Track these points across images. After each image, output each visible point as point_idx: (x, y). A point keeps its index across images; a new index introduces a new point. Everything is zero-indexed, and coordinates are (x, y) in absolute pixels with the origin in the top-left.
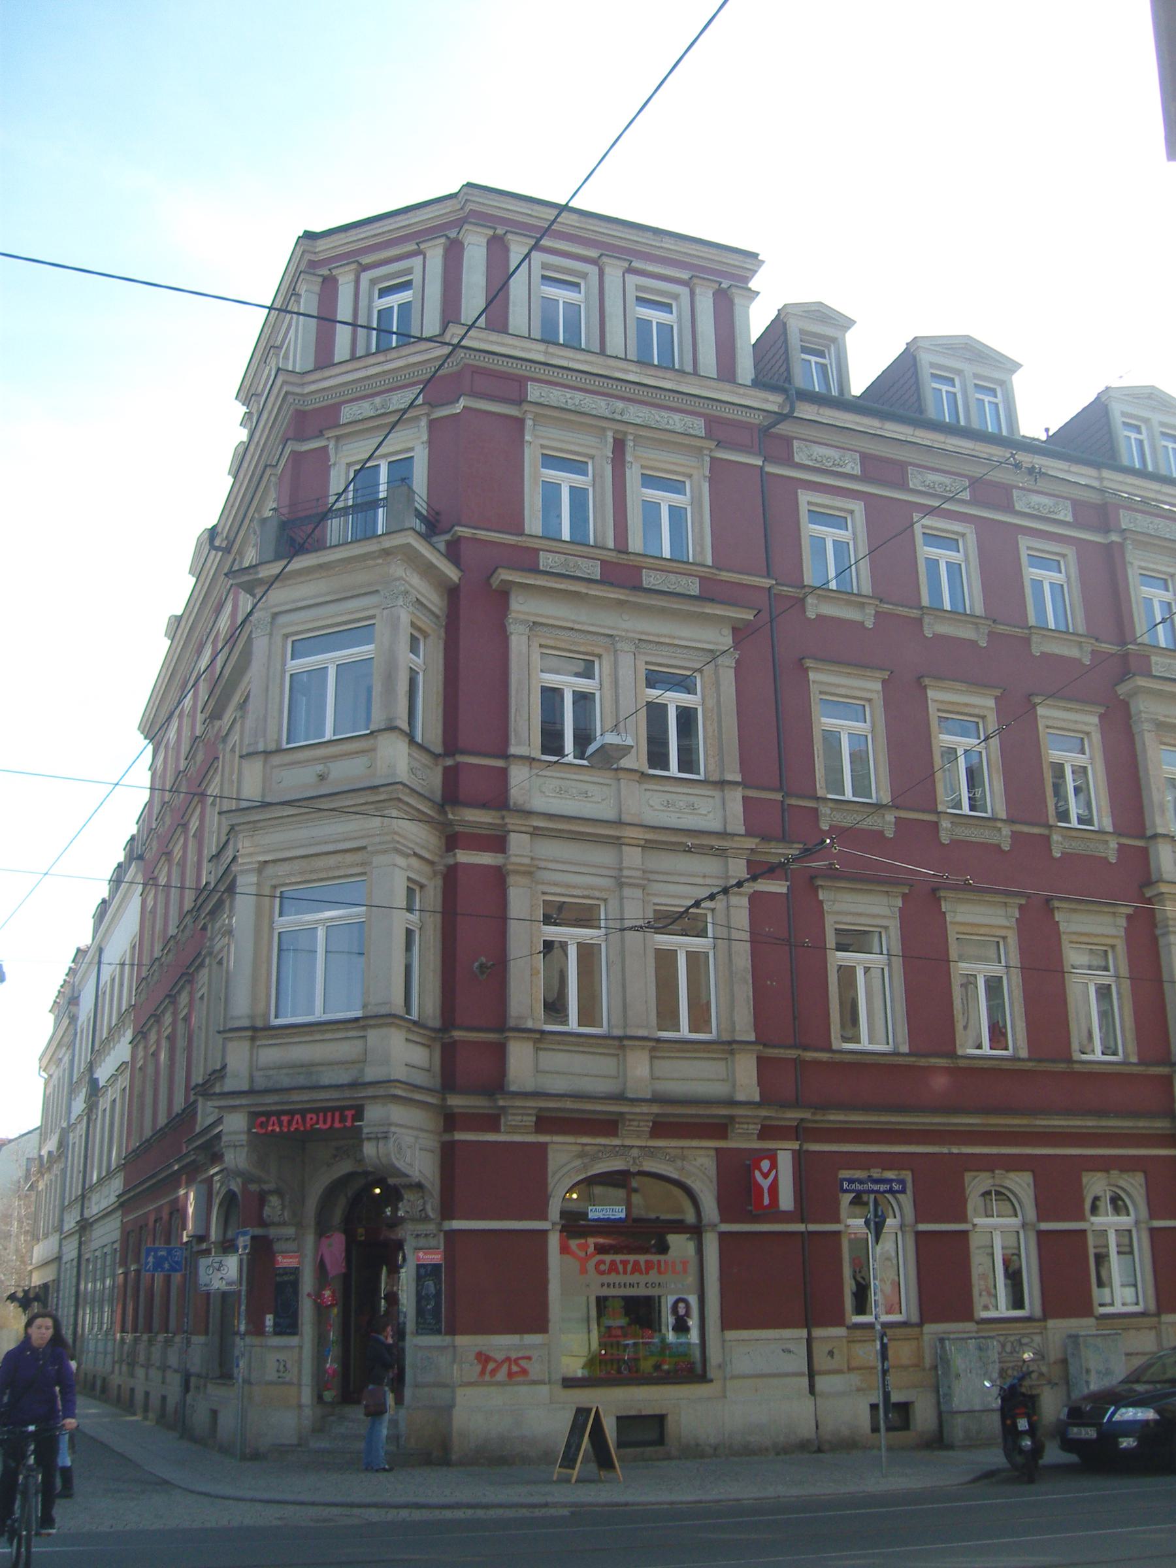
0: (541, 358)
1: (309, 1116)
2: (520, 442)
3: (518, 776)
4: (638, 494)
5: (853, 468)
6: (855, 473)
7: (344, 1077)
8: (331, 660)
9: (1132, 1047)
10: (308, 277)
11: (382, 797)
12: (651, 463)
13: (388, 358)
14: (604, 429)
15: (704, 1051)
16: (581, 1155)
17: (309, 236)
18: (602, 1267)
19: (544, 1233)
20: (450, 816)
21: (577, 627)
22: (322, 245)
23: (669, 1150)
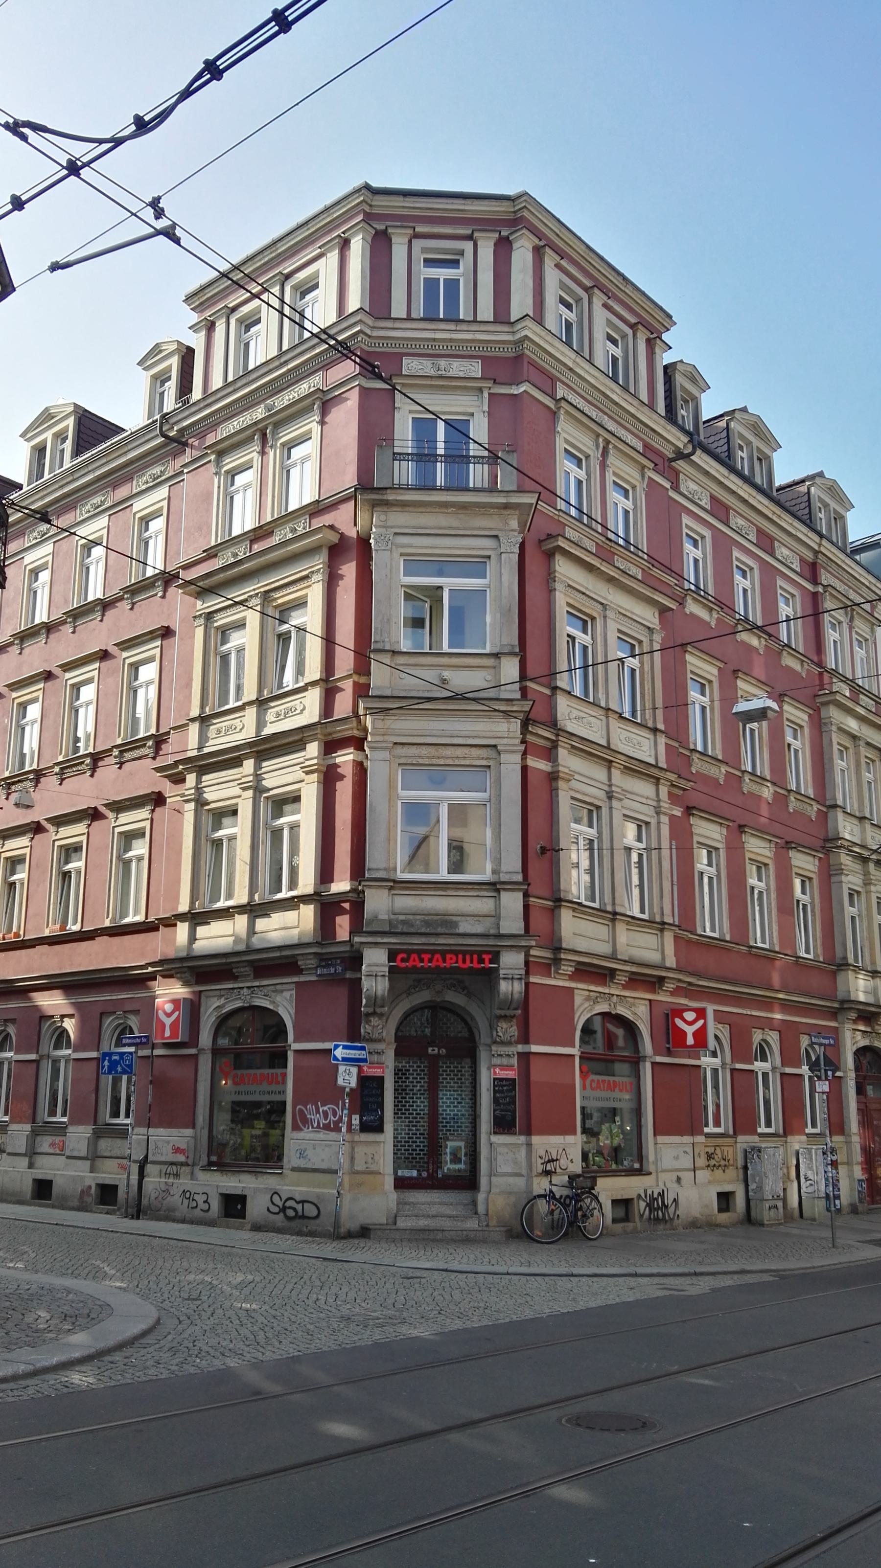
0: (570, 364)
1: (448, 956)
3: (563, 704)
8: (449, 583)
9: (820, 951)
16: (588, 998)
17: (367, 187)
19: (573, 1056)
21: (588, 593)
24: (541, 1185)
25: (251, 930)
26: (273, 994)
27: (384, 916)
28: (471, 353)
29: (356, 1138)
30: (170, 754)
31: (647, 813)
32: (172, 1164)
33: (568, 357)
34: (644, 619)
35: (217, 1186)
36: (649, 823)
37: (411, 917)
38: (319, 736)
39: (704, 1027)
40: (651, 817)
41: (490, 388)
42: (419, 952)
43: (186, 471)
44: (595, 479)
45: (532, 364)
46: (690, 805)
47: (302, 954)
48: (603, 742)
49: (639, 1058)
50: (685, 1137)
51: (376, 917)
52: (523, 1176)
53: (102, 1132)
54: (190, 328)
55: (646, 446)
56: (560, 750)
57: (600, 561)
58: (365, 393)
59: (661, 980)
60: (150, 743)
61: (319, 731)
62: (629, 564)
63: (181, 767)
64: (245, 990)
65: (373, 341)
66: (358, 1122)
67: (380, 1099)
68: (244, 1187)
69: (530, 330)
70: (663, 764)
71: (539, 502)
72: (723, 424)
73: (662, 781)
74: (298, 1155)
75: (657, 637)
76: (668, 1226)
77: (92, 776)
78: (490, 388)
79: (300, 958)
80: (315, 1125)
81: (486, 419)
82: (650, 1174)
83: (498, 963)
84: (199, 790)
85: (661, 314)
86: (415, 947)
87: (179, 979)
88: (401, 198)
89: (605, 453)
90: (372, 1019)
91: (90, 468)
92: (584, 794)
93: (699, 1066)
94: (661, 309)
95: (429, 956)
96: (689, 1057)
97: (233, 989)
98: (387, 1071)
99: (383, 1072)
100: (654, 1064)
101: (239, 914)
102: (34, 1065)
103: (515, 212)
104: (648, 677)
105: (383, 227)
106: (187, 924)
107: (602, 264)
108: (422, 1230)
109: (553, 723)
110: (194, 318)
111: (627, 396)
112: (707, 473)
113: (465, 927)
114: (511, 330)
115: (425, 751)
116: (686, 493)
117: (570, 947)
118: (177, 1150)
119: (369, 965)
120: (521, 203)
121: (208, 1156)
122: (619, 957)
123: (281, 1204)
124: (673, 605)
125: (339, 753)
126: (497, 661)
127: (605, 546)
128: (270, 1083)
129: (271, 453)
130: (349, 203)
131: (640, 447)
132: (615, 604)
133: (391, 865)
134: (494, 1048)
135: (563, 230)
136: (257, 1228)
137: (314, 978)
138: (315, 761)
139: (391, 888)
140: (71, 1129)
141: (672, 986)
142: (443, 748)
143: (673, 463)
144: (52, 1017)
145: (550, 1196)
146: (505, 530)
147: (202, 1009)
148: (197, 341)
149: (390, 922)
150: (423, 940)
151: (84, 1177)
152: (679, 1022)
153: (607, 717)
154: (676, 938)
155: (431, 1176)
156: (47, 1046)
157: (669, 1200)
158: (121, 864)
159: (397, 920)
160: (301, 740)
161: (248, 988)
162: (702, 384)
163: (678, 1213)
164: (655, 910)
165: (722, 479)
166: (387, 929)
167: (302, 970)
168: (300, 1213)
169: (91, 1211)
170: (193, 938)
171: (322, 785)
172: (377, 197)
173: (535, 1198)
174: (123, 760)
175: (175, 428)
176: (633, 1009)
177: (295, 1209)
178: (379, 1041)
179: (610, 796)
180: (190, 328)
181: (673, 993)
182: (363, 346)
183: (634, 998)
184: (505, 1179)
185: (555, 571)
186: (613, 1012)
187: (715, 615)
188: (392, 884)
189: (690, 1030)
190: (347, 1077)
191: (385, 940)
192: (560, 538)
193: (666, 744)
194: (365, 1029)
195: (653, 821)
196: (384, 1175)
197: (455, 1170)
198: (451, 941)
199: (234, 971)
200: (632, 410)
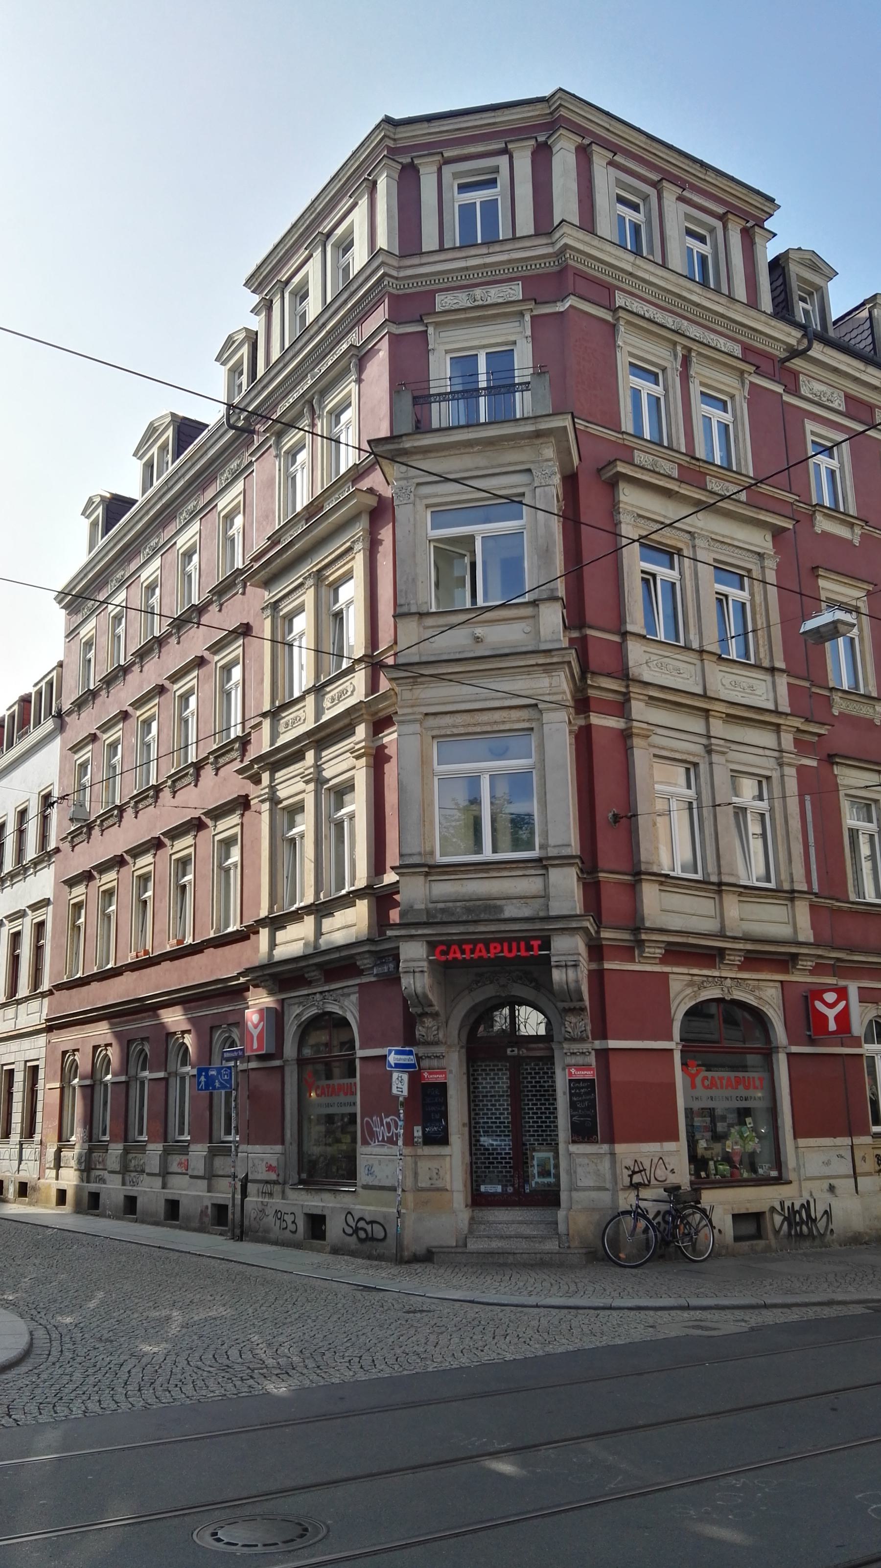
0: (629, 268)
1: (492, 946)
2: (613, 346)
3: (636, 652)
4: (701, 409)
5: (840, 405)
6: (841, 409)
7: (526, 912)
8: (480, 530)
10: (390, 162)
11: (555, 660)
12: (710, 382)
13: (491, 251)
14: (675, 344)
15: (772, 897)
16: (691, 984)
17: (388, 120)
18: (707, 1083)
19: (671, 1051)
20: (589, 682)
22: (403, 132)
23: (749, 982)
24: (626, 1201)
25: (318, 933)
26: (342, 998)
27: (420, 906)
28: (510, 276)
29: (420, 1151)
30: (253, 753)
31: (766, 765)
32: (267, 1182)
33: (626, 261)
34: (751, 544)
35: (302, 1206)
36: (770, 777)
37: (451, 904)
38: (365, 717)
39: (846, 1009)
40: (772, 770)
41: (532, 310)
42: (460, 943)
43: (254, 459)
44: (675, 393)
45: (579, 274)
46: (832, 753)
47: (359, 954)
48: (699, 690)
49: (771, 1049)
50: (838, 1139)
51: (412, 907)
52: (607, 1190)
53: (219, 1151)
54: (252, 312)
55: (746, 348)
56: (634, 703)
57: (678, 483)
58: (395, 340)
59: (795, 957)
60: (237, 745)
61: (364, 711)
62: (727, 484)
63: (256, 766)
64: (318, 995)
65: (402, 283)
66: (420, 1134)
67: (443, 1108)
68: (323, 1207)
69: (571, 237)
70: (785, 707)
71: (518, 416)
72: (865, 314)
73: (783, 727)
74: (367, 1172)
75: (771, 563)
76: (817, 1242)
77: (196, 786)
78: (532, 310)
79: (358, 957)
80: (380, 1139)
81: (530, 345)
82: (790, 1182)
83: (550, 950)
84: (272, 788)
85: (759, 198)
86: (455, 938)
87: (264, 987)
88: (426, 125)
89: (686, 362)
90: (425, 1020)
91: (180, 474)
92: (672, 750)
93: (862, 1055)
94: (758, 193)
95: (471, 946)
96: (842, 1045)
97: (308, 995)
98: (450, 1076)
99: (445, 1078)
100: (790, 1055)
101: (307, 915)
102: (163, 1083)
103: (551, 113)
104: (761, 610)
105: (409, 160)
106: (267, 929)
107: (671, 153)
108: (492, 1253)
109: (624, 674)
110: (256, 298)
111: (710, 295)
112: (835, 370)
113: (510, 911)
114: (549, 241)
115: (459, 719)
116: (811, 396)
117: (658, 925)
118: (270, 1168)
119: (406, 961)
120: (555, 102)
121: (299, 1174)
122: (728, 934)
123: (353, 1225)
124: (788, 524)
125: (386, 732)
126: (536, 609)
127: (692, 466)
128: (747, 1088)
129: (319, 424)
130: (372, 142)
131: (737, 351)
132: (707, 531)
133: (428, 849)
134: (566, 1046)
135: (614, 122)
136: (336, 1251)
137: (373, 979)
138: (363, 744)
139: (427, 874)
140: (193, 1147)
141: (809, 963)
142: (479, 713)
143: (787, 364)
144: (175, 1033)
145: (638, 1213)
146: (538, 462)
147: (286, 1018)
148: (256, 323)
149: (428, 911)
150: (461, 929)
151: (203, 1196)
152: (819, 1005)
153: (702, 660)
154: (813, 907)
155: (517, 1192)
156: (174, 1064)
157: (817, 1211)
158: (223, 872)
159: (436, 909)
160: (350, 724)
161: (321, 993)
162: (826, 271)
163: (830, 1227)
164: (783, 877)
165: (857, 375)
166: (425, 919)
167: (363, 970)
168: (370, 1235)
169: (208, 1232)
170: (273, 945)
171: (372, 770)
172: (400, 129)
173: (619, 1215)
174: (218, 766)
175: (242, 417)
176: (757, 993)
177: (365, 1230)
178: (437, 1043)
179: (709, 751)
180: (252, 312)
181: (812, 972)
182: (391, 290)
183: (758, 980)
184: (587, 1193)
185: (619, 502)
186: (728, 998)
187: (858, 531)
188: (426, 869)
189: (831, 1014)
190: (400, 1085)
191: (420, 932)
192: (618, 463)
193: (788, 683)
194: (420, 1031)
195: (775, 775)
196: (452, 1192)
197: (544, 1184)
198: (493, 928)
199: (306, 975)
200: (720, 309)
